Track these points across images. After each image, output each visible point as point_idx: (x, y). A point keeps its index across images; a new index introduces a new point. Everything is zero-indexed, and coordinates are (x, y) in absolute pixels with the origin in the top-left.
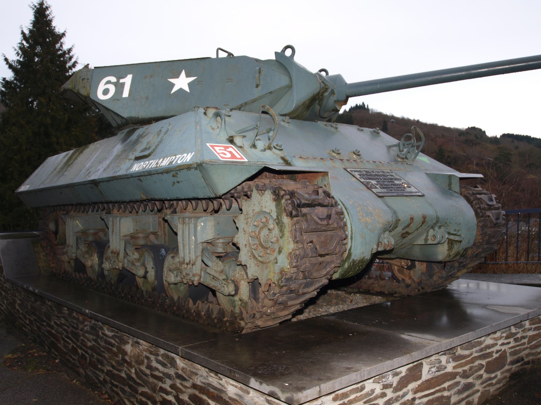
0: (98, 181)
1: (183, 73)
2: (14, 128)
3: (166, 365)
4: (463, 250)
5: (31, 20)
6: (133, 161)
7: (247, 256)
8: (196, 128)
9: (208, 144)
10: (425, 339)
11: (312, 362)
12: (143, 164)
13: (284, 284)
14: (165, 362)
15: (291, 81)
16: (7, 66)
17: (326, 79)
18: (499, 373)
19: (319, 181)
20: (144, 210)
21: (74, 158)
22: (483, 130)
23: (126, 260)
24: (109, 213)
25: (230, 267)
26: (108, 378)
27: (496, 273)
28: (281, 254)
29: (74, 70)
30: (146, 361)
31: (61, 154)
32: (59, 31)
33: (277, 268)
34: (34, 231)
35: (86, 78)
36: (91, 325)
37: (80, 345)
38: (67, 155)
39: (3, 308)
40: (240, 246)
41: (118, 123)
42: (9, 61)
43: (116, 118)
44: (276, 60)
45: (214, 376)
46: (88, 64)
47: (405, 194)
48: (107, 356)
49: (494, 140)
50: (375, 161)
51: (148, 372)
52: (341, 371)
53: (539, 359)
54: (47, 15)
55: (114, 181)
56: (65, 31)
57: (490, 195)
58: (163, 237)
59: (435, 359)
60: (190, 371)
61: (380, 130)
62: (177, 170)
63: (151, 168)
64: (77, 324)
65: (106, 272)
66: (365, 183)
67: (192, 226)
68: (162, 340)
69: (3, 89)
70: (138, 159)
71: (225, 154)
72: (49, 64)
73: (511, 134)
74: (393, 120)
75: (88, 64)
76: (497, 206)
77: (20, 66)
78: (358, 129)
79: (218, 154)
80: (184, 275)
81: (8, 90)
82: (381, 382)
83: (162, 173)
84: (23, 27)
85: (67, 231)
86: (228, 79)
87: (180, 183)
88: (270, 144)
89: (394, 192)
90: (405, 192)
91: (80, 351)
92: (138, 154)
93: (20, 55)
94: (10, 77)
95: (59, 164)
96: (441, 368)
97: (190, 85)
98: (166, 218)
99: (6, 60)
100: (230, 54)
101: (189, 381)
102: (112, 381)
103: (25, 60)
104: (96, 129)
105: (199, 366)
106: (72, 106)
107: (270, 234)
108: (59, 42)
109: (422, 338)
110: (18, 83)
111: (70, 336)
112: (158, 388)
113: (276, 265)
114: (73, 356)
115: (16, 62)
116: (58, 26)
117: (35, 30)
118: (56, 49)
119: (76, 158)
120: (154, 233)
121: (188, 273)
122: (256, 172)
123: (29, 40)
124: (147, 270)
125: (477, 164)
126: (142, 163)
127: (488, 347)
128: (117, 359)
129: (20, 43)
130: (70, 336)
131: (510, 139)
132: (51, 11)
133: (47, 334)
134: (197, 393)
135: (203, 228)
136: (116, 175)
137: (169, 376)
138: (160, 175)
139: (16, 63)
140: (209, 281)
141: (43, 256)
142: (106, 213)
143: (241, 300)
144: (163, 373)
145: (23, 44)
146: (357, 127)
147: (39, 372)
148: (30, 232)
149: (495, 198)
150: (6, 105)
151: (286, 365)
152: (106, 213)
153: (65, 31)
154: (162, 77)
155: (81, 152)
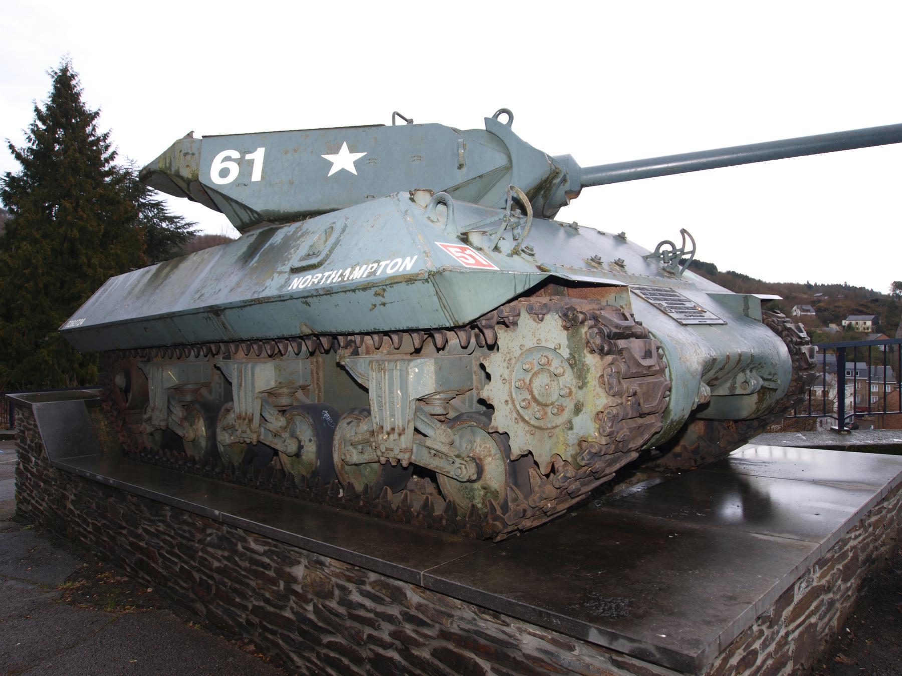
0: (223, 308)
2: (25, 243)
3: (383, 599)
5: (49, 92)
6: (286, 275)
7: (509, 418)
9: (437, 243)
12: (312, 278)
13: (587, 462)
14: (378, 594)
15: (510, 161)
16: (14, 155)
18: (852, 580)
19: (610, 297)
20: (296, 352)
23: (262, 430)
24: (228, 357)
25: (461, 437)
26: (255, 620)
28: (580, 415)
30: (337, 592)
32: (91, 109)
33: (572, 437)
35: (190, 152)
36: (220, 534)
37: (198, 565)
38: (148, 272)
39: (41, 508)
40: (495, 403)
41: (244, 220)
48: (253, 583)
51: (342, 610)
58: (317, 392)
60: (434, 609)
62: (386, 285)
63: (332, 283)
64: (190, 532)
65: (222, 448)
67: (396, 374)
68: (381, 560)
69: (7, 189)
70: (295, 271)
72: (78, 155)
75: (192, 132)
80: (383, 450)
83: (354, 291)
85: (151, 388)
86: (414, 156)
88: (518, 245)
91: (197, 576)
93: (32, 141)
97: (356, 164)
98: (343, 363)
100: (410, 121)
101: (433, 626)
102: (265, 623)
105: (458, 602)
107: (552, 382)
111: (176, 550)
112: (365, 637)
113: (570, 432)
114: (182, 583)
115: (26, 151)
116: (89, 101)
119: (167, 276)
120: (304, 388)
121: (391, 447)
122: (535, 284)
124: (302, 444)
128: (275, 588)
129: (32, 125)
130: (176, 550)
133: (129, 548)
134: (451, 646)
135: (418, 376)
136: (261, 297)
137: (390, 619)
139: (26, 153)
140: (428, 459)
141: (105, 425)
142: (224, 358)
143: (484, 488)
144: (377, 614)
145: (37, 126)
152: (224, 358)
154: (312, 152)
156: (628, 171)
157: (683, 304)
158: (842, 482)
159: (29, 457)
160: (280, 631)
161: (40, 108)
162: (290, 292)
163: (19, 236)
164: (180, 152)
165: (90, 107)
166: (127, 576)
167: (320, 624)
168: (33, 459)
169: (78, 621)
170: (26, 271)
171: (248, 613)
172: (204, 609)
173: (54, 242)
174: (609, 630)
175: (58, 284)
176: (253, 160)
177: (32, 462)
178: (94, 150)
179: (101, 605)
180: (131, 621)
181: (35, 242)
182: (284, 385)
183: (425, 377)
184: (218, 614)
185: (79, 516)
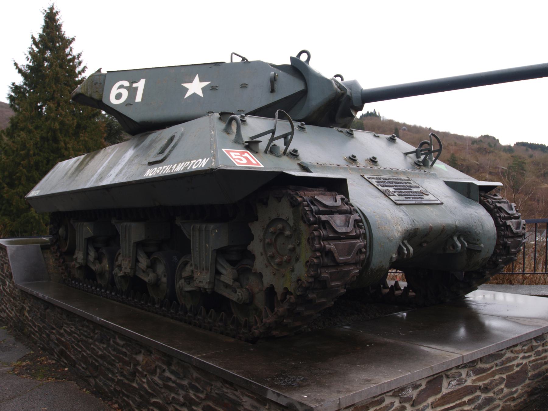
1: (197, 77)
2: (22, 132)
4: (483, 259)
9: (223, 150)
11: (329, 373)
12: (157, 169)
16: (17, 70)
17: (342, 84)
18: (519, 387)
21: (85, 163)
22: (496, 138)
29: (83, 75)
31: (72, 159)
34: (43, 237)
38: (78, 160)
39: (11, 315)
45: (229, 387)
46: (101, 69)
47: (424, 202)
48: (117, 365)
49: (508, 149)
50: (392, 168)
51: (160, 382)
52: (360, 384)
54: (57, 20)
59: (455, 372)
61: (396, 136)
66: (383, 190)
70: (151, 164)
71: (241, 160)
72: (58, 69)
73: (525, 143)
74: (405, 128)
75: (101, 69)
76: (517, 215)
77: (29, 71)
78: (375, 135)
79: (234, 159)
81: (17, 95)
82: (400, 394)
89: (412, 200)
93: (29, 60)
94: (20, 82)
95: (70, 169)
96: (462, 381)
97: (203, 89)
99: (16, 64)
100: (244, 59)
103: (35, 65)
104: (105, 135)
106: (81, 112)
108: (69, 47)
109: (442, 350)
110: (27, 88)
115: (25, 67)
116: (67, 31)
117: (45, 34)
118: (66, 54)
119: (87, 163)
121: (202, 281)
123: (39, 44)
125: (490, 173)
126: (156, 169)
127: (510, 360)
128: (128, 368)
129: (29, 48)
131: (525, 148)
137: (182, 387)
139: (25, 68)
145: (33, 49)
146: (374, 133)
147: (48, 380)
148: (40, 238)
149: (515, 207)
150: (15, 110)
151: (303, 376)
154: (175, 81)
155: (93, 157)
157: (411, 190)
159: (5, 282)
160: (131, 395)
161: (34, 36)
163: (19, 128)
166: (55, 360)
167: (149, 390)
168: (8, 283)
169: (19, 384)
170: (22, 152)
171: (115, 383)
172: (94, 382)
173: (42, 132)
174: (277, 392)
175: (45, 161)
177: (7, 285)
178: (71, 65)
179: (35, 376)
180: (50, 386)
181: (30, 132)
184: (100, 384)
185: (31, 321)
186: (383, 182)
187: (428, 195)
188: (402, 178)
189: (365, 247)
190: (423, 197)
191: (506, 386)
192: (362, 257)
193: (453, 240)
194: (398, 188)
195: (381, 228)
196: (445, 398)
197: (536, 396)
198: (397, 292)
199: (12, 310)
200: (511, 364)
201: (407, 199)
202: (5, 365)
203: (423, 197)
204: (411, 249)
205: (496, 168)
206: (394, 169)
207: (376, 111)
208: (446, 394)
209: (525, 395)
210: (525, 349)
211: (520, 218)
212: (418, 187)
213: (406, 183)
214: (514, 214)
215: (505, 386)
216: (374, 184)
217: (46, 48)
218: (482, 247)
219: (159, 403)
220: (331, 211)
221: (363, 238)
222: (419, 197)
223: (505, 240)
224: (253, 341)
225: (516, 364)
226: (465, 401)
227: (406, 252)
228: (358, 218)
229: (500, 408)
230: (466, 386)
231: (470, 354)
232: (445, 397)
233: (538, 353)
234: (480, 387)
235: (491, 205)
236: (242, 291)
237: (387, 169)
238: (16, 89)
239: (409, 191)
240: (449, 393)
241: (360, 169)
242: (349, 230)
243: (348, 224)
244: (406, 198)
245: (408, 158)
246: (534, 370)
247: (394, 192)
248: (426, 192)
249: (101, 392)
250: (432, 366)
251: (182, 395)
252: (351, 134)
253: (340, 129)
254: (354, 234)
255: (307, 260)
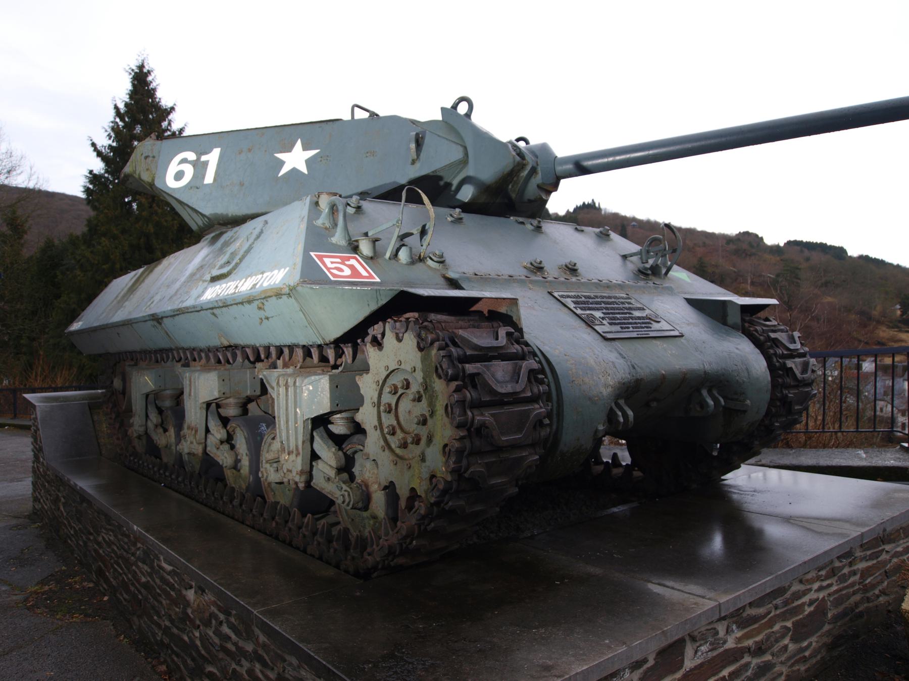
2: (103, 239)
8: (299, 227)
10: (689, 593)
16: (95, 154)
18: (814, 639)
21: (142, 279)
22: (760, 236)
27: (791, 447)
32: (167, 104)
35: (151, 155)
38: (136, 274)
41: (199, 224)
42: (98, 147)
43: (194, 216)
44: (443, 121)
48: (164, 602)
49: (776, 249)
50: (601, 279)
53: (877, 606)
55: (180, 316)
56: (175, 105)
57: (790, 333)
61: (611, 230)
63: (228, 295)
66: (583, 316)
70: (215, 279)
73: (799, 241)
74: (635, 224)
76: (802, 351)
77: (112, 154)
78: (576, 229)
79: (328, 269)
83: (242, 303)
84: (117, 99)
86: (367, 153)
87: (270, 319)
89: (632, 331)
90: (652, 331)
92: (216, 272)
93: (112, 139)
96: (719, 643)
97: (309, 162)
99: (93, 145)
100: (373, 115)
109: (683, 591)
110: (110, 176)
113: (424, 464)
115: (107, 148)
116: (165, 97)
121: (290, 469)
122: (388, 300)
125: (753, 283)
126: (218, 287)
127: (798, 595)
129: (112, 122)
131: (798, 248)
132: (155, 76)
136: (183, 306)
138: (240, 306)
145: (117, 123)
147: (73, 618)
149: (799, 337)
150: (95, 208)
153: (175, 105)
156: (605, 160)
158: (818, 519)
162: (201, 302)
164: (142, 155)
165: (166, 102)
166: (93, 582)
167: (203, 652)
170: (104, 267)
176: (208, 161)
182: (228, 396)
183: (320, 395)
186: (584, 303)
187: (658, 322)
188: (617, 295)
189: (549, 415)
190: (650, 325)
191: (792, 640)
192: (544, 432)
193: (701, 394)
194: (610, 311)
195: (576, 383)
196: (690, 677)
197: (840, 649)
198: (616, 471)
199: (47, 499)
200: (799, 602)
201: (624, 330)
202: (17, 592)
203: (650, 325)
204: (630, 413)
205: (760, 276)
206: (604, 281)
207: (595, 201)
208: (691, 670)
209: (822, 651)
210: (822, 575)
211: (808, 356)
212: (644, 309)
213: (623, 303)
214: (797, 349)
215: (790, 640)
216: (569, 306)
217: (135, 121)
218: (747, 405)
219: (216, 675)
220: (486, 355)
221: (545, 400)
222: (643, 325)
223: (784, 392)
224: (364, 575)
225: (808, 601)
226: (725, 676)
227: (621, 420)
228: (536, 366)
229: (783, 678)
230: (726, 650)
231: (731, 599)
232: (690, 675)
233: (843, 579)
234: (749, 649)
235: (761, 335)
236: (351, 488)
237: (593, 281)
238: (94, 178)
239: (628, 315)
240: (696, 667)
241: (547, 282)
242: (518, 388)
243: (517, 378)
244: (622, 328)
245: (628, 263)
246: (836, 607)
247: (603, 318)
248: (656, 317)
249: (144, 641)
250: (665, 629)
251: (246, 668)
252: (538, 228)
253: (521, 219)
254: (529, 394)
255: (446, 443)
